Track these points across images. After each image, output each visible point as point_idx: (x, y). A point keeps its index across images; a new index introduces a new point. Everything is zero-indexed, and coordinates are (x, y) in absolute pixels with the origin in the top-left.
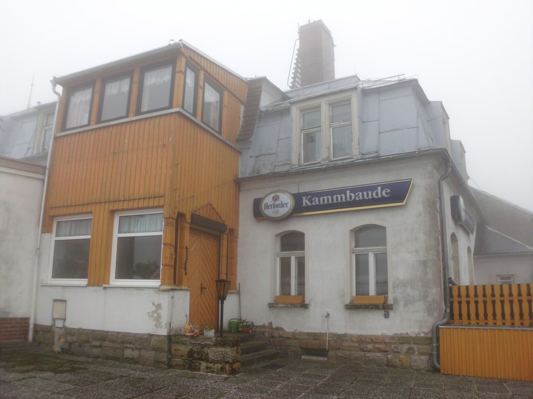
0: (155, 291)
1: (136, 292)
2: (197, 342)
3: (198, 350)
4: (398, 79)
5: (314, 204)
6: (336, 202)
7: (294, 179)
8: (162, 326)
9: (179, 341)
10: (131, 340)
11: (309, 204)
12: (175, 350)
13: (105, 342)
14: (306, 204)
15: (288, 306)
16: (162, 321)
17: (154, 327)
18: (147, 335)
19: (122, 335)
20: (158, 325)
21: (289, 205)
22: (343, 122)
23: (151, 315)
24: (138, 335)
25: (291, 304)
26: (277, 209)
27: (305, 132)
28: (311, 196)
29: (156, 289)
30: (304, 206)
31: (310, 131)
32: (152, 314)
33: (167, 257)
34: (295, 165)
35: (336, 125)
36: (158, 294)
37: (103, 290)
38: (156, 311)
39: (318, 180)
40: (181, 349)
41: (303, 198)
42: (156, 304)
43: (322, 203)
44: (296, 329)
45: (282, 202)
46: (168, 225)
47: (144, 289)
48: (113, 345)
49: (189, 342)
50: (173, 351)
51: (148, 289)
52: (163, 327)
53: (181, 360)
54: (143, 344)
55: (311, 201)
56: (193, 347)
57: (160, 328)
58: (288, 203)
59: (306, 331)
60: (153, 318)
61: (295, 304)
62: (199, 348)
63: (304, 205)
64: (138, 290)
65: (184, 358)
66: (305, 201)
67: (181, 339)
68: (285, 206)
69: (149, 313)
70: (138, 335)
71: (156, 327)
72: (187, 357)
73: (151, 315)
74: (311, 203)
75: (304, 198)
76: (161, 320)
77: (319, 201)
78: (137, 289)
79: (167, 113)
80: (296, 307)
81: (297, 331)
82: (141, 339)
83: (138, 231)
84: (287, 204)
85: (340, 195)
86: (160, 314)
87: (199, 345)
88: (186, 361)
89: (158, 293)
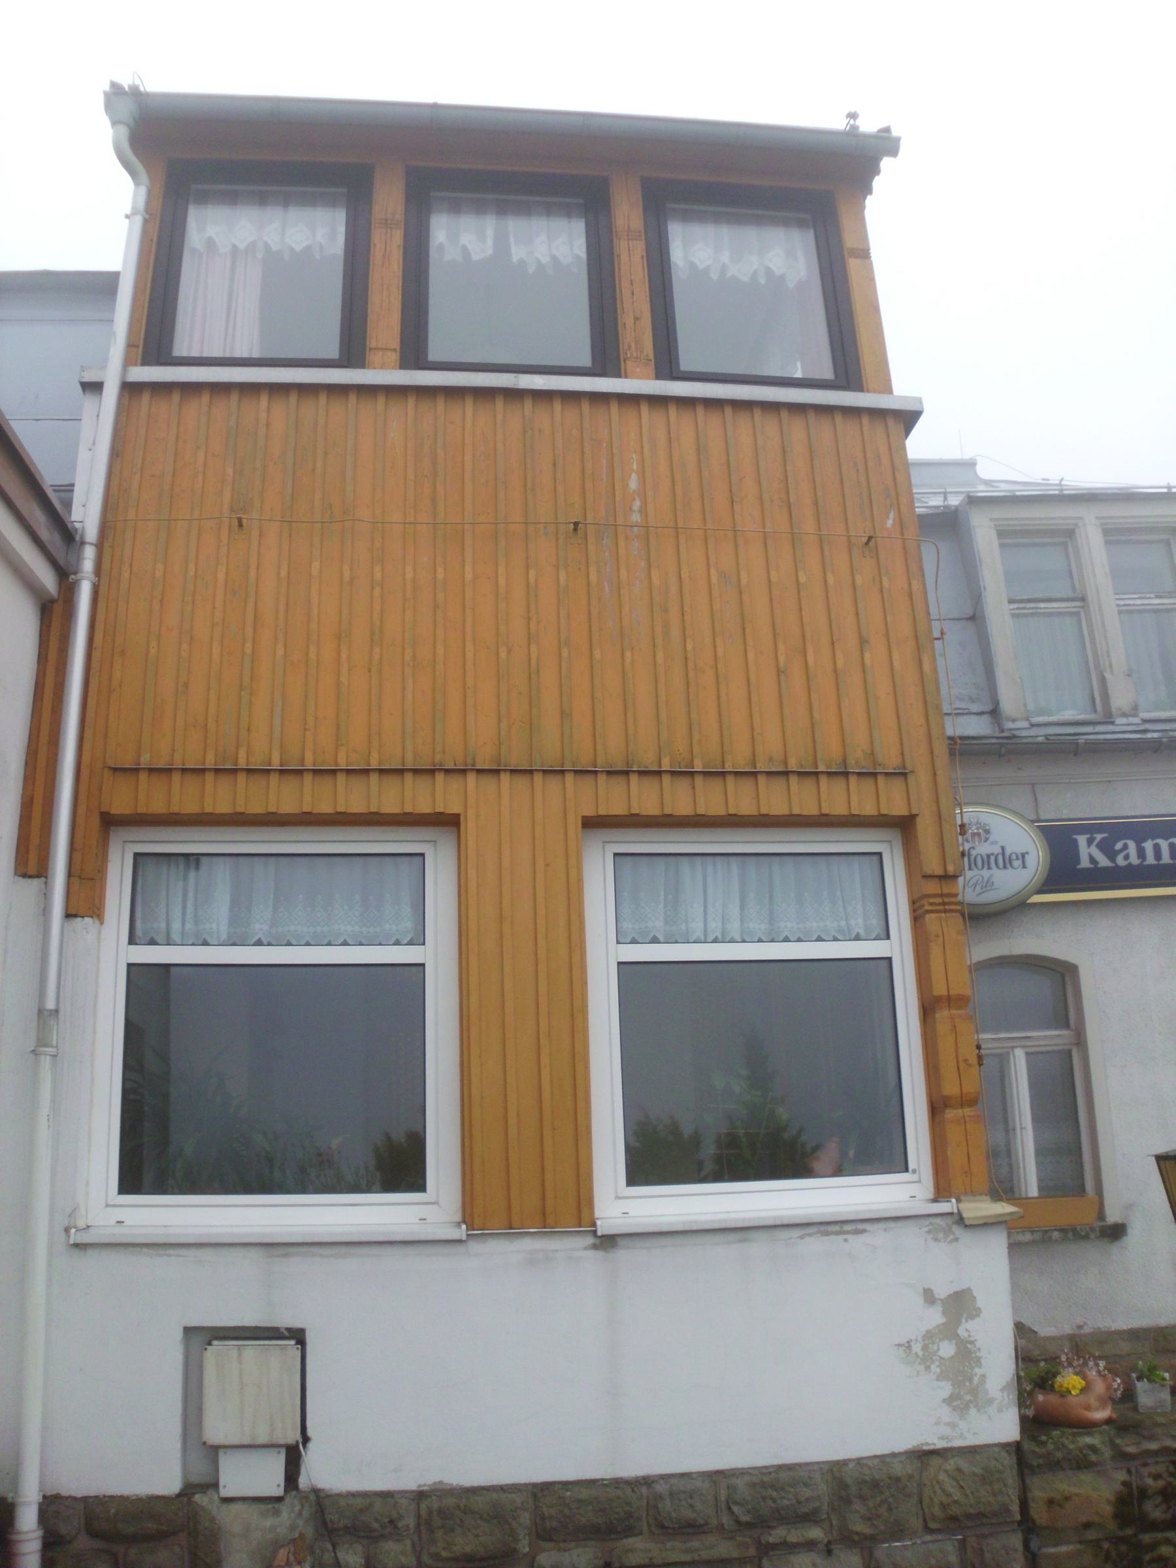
0: (929, 1232)
1: (815, 1245)
2: (1154, 1446)
3: (1161, 1483)
4: (941, 503)
5: (1120, 861)
6: (1155, 862)
7: (1020, 769)
8: (991, 1401)
9: (1059, 1455)
10: (818, 1504)
11: (1104, 861)
12: (1051, 1502)
13: (630, 1542)
14: (1092, 860)
15: (1050, 1238)
16: (983, 1376)
17: (946, 1413)
18: (903, 1458)
19: (753, 1485)
20: (968, 1397)
21: (1031, 861)
22: (1157, 597)
23: (920, 1353)
24: (851, 1465)
25: (1062, 1230)
26: (986, 873)
27: (1017, 609)
28: (1106, 835)
29: (938, 1221)
30: (1148, 865)
31: (1040, 608)
32: (925, 1348)
33: (966, 1061)
34: (1014, 720)
35: (1131, 602)
36: (951, 1242)
37: (592, 1253)
38: (949, 1331)
39: (1110, 781)
40: (1077, 1495)
41: (1076, 841)
42: (942, 1292)
43: (1150, 860)
44: (1079, 1321)
45: (1003, 848)
46: (945, 911)
47: (867, 1226)
48: (687, 1551)
49: (1107, 1453)
50: (1039, 1513)
51: (892, 1224)
52: (995, 1405)
53: (1079, 1546)
54: (890, 1509)
55: (1111, 854)
56: (1129, 1472)
57: (979, 1410)
58: (1027, 853)
59: (1122, 1323)
60: (933, 1367)
61: (1078, 1228)
62: (1161, 1469)
63: (1085, 863)
64: (827, 1234)
65: (1091, 1535)
66: (1088, 852)
67: (1071, 1446)
68: (1016, 863)
69: (908, 1346)
70: (851, 1465)
71: (955, 1409)
72: (1112, 1526)
73: (920, 1353)
74: (1113, 859)
75: (1082, 840)
76: (977, 1370)
77: (1141, 853)
78: (819, 1232)
79: (832, 403)
80: (1086, 1237)
81: (1086, 1330)
82: (875, 1485)
83: (176, 937)
84: (1023, 855)
85: (1166, 839)
86: (972, 1342)
87: (1160, 1459)
88: (1106, 1545)
89: (952, 1237)
